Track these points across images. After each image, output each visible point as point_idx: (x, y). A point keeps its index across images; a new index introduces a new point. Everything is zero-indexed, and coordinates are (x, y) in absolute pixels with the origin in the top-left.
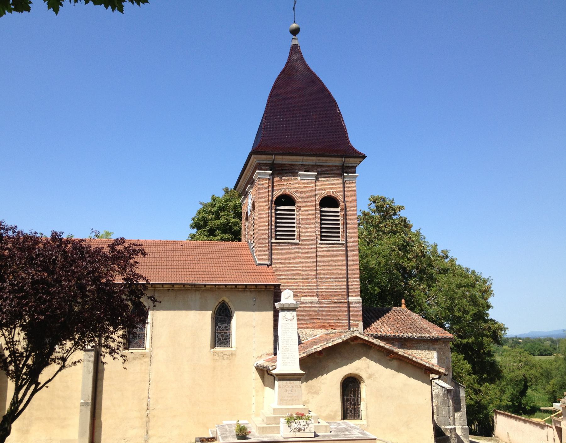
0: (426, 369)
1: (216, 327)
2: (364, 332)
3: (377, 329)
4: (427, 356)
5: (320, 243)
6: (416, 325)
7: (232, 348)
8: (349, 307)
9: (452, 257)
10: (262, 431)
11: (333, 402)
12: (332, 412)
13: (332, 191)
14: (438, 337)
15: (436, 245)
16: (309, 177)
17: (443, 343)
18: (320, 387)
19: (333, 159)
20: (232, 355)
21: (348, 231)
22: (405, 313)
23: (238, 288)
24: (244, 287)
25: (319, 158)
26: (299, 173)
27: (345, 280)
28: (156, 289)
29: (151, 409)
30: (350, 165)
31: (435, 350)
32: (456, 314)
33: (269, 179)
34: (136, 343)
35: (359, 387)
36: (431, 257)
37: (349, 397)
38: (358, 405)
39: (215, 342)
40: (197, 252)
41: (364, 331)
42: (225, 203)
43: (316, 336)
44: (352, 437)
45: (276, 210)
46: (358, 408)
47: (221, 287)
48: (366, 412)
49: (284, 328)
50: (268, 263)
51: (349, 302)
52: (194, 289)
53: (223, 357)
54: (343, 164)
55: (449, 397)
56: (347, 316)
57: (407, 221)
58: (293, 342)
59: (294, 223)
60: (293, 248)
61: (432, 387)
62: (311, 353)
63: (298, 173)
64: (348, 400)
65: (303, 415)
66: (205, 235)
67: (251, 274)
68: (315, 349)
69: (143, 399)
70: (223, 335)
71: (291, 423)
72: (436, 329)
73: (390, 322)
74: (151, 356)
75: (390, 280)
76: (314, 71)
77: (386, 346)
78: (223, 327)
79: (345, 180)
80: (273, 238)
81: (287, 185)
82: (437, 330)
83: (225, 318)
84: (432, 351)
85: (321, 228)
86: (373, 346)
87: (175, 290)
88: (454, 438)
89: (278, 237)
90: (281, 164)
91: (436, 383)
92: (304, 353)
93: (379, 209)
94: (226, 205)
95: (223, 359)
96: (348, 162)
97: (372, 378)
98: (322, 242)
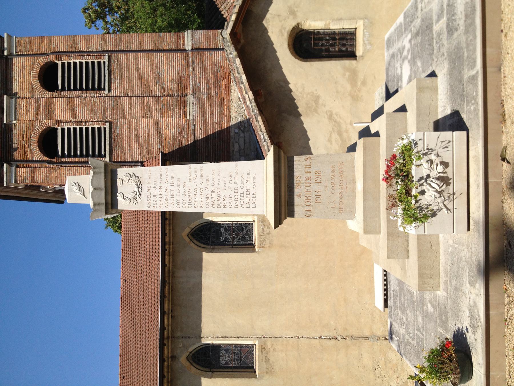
5: (109, 91)
7: (254, 221)
8: (199, 49)
11: (330, 73)
12: (345, 75)
13: (32, 74)
16: (12, 108)
18: (309, 94)
21: (90, 50)
27: (161, 54)
28: (170, 335)
29: (335, 334)
33: (18, 166)
34: (247, 357)
38: (334, 33)
39: (246, 245)
45: (63, 156)
46: (340, 33)
48: (346, 21)
49: (160, 201)
51: (193, 50)
53: (267, 233)
56: (212, 53)
58: (195, 178)
60: (117, 130)
62: (257, 108)
64: (327, 50)
68: (251, 102)
69: (322, 346)
70: (236, 235)
71: (421, 209)
74: (264, 337)
78: (226, 234)
81: (25, 139)
83: (214, 232)
85: (87, 89)
87: (172, 307)
92: (257, 120)
93: (101, 16)
97: (296, 10)
98: (107, 88)
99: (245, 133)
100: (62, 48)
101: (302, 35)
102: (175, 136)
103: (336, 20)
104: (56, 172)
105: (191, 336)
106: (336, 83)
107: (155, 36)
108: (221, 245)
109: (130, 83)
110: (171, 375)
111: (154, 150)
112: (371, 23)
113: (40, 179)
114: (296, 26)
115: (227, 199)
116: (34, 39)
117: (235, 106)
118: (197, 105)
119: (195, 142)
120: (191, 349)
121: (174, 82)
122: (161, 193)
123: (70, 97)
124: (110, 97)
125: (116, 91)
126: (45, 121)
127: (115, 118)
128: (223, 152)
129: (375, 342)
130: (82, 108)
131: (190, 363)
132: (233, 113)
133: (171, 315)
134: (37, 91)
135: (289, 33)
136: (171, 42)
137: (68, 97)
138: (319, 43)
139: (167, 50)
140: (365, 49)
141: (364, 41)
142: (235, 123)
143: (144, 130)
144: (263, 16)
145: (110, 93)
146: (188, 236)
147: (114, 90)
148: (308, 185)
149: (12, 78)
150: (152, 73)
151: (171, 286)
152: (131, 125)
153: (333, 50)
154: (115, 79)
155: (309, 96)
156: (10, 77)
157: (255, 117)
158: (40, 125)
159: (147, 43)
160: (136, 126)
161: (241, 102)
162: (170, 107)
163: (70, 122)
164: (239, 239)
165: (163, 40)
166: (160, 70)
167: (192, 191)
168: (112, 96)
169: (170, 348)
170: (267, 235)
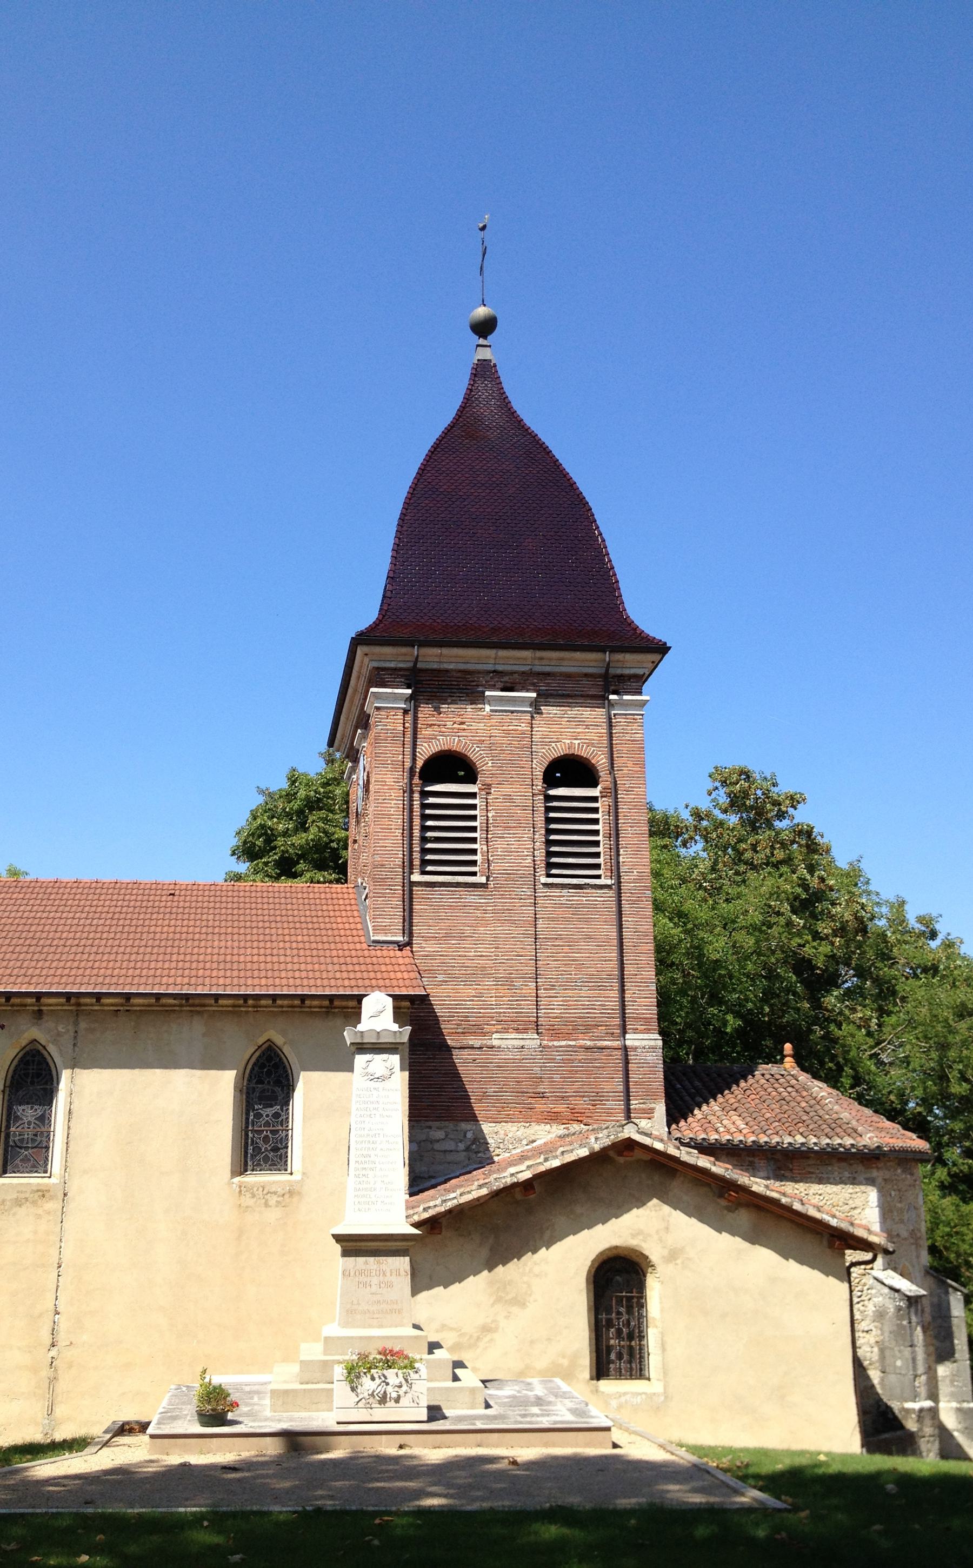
0: (833, 1236)
1: (248, 1114)
2: (670, 1133)
3: (707, 1124)
4: (850, 1202)
5: (545, 885)
6: (821, 1113)
7: (291, 1174)
8: (627, 1062)
9: (949, 934)
10: (283, 1403)
11: (566, 1327)
12: (564, 1357)
13: (577, 742)
14: (878, 1147)
15: (903, 903)
17: (899, 1165)
18: (529, 1286)
19: (578, 655)
20: (291, 1193)
21: (621, 851)
22: (793, 1082)
23: (310, 1007)
24: (326, 1003)
25: (539, 654)
26: (487, 693)
27: (616, 985)
30: (627, 672)
31: (874, 1185)
32: (953, 1091)
33: (406, 712)
34: (24, 1161)
35: (640, 1286)
36: (889, 935)
37: (614, 1315)
38: (641, 1337)
39: (246, 1156)
40: (211, 911)
41: (669, 1128)
42: (322, 790)
43: (533, 1141)
44: (541, 1422)
45: (425, 794)
46: (641, 1349)
47: (263, 1002)
48: (661, 1359)
50: (401, 939)
51: (625, 1049)
52: (188, 1008)
53: (267, 1200)
54: (607, 670)
55: (914, 1319)
56: (621, 1088)
57: (814, 834)
59: (474, 829)
60: (472, 897)
61: (850, 1286)
62: (502, 1186)
63: (484, 692)
64: (610, 1324)
65: (400, 1354)
66: (268, 876)
67: (350, 967)
68: (512, 1175)
69: (40, 1316)
71: (358, 1377)
72: (880, 1125)
73: (747, 1105)
74: (65, 1195)
75: (768, 995)
76: (532, 428)
77: (714, 1169)
79: (613, 712)
80: (416, 871)
81: (455, 726)
82: (881, 1130)
83: (273, 1092)
84: (863, 1188)
85: (549, 843)
86: (679, 1167)
87: (136, 1010)
88: (930, 1436)
89: (429, 868)
90: (439, 671)
91: (876, 1279)
92: (480, 1187)
93: (736, 802)
94: (327, 795)
95: (266, 1205)
96: (620, 665)
97: (679, 1261)
98: (550, 880)
99: (464, 1153)
100: (623, 798)
101: (637, 1273)
102: (460, 1009)
103: (662, 1340)
104: (394, 782)
105: (77, 1049)
106: (549, 1339)
107: (649, 975)
108: (247, 1106)
109: (561, 924)
110: (6, 1010)
111: (433, 966)
112: (658, 1408)
113: (382, 753)
114: (650, 1262)
115: (364, 1179)
116: (639, 748)
117: (518, 1133)
118: (520, 1055)
119: (449, 1049)
120: (52, 1049)
121: (564, 1009)
122: (372, 1103)
123: (533, 810)
124: (535, 885)
125: (545, 896)
126: (490, 764)
127: (494, 895)
128: (428, 1106)
129: (42, 1429)
130: (514, 834)
131: (25, 1047)
132: (505, 1128)
133: (119, 1010)
134: (544, 750)
135: (637, 1249)
136: (639, 1006)
137: (533, 807)
138: (622, 1307)
139: (624, 997)
140: (609, 1396)
141: (625, 1394)
142: (485, 1132)
143: (472, 948)
144: (665, 1200)
145: (541, 886)
146: (269, 1040)
147: (548, 894)
148: (378, 1272)
149: (569, 706)
150: (580, 967)
151: (175, 1008)
152: (481, 924)
153: (611, 1336)
154: (567, 896)
155: (525, 1286)
156: (571, 703)
157: (486, 1183)
158: (481, 754)
159: (636, 960)
160: (481, 934)
161: (527, 1145)
162: (517, 1000)
163: (487, 811)
164: (257, 1143)
165: (643, 990)
166: (586, 982)
167: (374, 1139)
168: (535, 889)
169: (59, 1008)
170: (264, 1201)
